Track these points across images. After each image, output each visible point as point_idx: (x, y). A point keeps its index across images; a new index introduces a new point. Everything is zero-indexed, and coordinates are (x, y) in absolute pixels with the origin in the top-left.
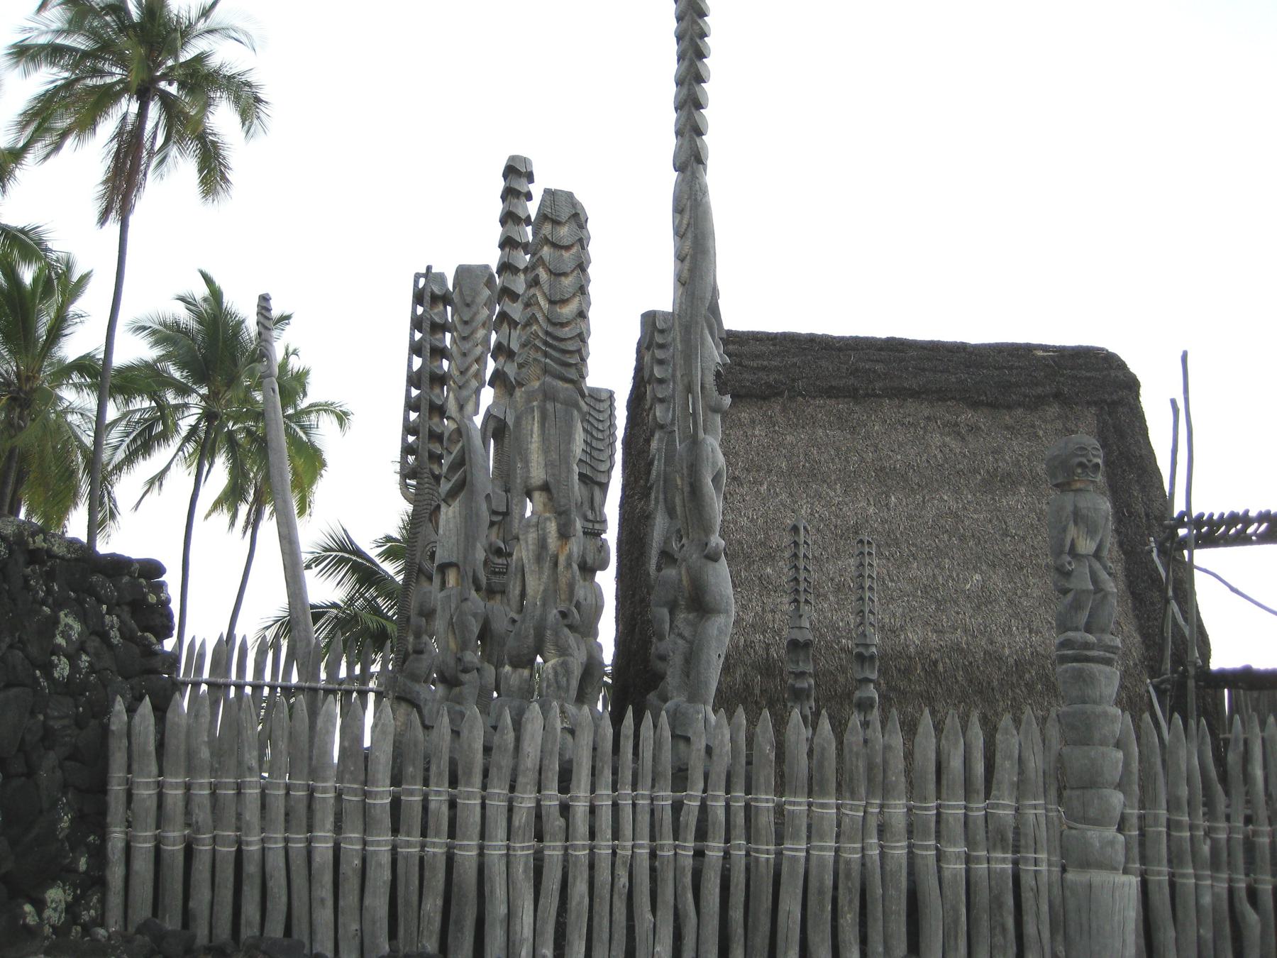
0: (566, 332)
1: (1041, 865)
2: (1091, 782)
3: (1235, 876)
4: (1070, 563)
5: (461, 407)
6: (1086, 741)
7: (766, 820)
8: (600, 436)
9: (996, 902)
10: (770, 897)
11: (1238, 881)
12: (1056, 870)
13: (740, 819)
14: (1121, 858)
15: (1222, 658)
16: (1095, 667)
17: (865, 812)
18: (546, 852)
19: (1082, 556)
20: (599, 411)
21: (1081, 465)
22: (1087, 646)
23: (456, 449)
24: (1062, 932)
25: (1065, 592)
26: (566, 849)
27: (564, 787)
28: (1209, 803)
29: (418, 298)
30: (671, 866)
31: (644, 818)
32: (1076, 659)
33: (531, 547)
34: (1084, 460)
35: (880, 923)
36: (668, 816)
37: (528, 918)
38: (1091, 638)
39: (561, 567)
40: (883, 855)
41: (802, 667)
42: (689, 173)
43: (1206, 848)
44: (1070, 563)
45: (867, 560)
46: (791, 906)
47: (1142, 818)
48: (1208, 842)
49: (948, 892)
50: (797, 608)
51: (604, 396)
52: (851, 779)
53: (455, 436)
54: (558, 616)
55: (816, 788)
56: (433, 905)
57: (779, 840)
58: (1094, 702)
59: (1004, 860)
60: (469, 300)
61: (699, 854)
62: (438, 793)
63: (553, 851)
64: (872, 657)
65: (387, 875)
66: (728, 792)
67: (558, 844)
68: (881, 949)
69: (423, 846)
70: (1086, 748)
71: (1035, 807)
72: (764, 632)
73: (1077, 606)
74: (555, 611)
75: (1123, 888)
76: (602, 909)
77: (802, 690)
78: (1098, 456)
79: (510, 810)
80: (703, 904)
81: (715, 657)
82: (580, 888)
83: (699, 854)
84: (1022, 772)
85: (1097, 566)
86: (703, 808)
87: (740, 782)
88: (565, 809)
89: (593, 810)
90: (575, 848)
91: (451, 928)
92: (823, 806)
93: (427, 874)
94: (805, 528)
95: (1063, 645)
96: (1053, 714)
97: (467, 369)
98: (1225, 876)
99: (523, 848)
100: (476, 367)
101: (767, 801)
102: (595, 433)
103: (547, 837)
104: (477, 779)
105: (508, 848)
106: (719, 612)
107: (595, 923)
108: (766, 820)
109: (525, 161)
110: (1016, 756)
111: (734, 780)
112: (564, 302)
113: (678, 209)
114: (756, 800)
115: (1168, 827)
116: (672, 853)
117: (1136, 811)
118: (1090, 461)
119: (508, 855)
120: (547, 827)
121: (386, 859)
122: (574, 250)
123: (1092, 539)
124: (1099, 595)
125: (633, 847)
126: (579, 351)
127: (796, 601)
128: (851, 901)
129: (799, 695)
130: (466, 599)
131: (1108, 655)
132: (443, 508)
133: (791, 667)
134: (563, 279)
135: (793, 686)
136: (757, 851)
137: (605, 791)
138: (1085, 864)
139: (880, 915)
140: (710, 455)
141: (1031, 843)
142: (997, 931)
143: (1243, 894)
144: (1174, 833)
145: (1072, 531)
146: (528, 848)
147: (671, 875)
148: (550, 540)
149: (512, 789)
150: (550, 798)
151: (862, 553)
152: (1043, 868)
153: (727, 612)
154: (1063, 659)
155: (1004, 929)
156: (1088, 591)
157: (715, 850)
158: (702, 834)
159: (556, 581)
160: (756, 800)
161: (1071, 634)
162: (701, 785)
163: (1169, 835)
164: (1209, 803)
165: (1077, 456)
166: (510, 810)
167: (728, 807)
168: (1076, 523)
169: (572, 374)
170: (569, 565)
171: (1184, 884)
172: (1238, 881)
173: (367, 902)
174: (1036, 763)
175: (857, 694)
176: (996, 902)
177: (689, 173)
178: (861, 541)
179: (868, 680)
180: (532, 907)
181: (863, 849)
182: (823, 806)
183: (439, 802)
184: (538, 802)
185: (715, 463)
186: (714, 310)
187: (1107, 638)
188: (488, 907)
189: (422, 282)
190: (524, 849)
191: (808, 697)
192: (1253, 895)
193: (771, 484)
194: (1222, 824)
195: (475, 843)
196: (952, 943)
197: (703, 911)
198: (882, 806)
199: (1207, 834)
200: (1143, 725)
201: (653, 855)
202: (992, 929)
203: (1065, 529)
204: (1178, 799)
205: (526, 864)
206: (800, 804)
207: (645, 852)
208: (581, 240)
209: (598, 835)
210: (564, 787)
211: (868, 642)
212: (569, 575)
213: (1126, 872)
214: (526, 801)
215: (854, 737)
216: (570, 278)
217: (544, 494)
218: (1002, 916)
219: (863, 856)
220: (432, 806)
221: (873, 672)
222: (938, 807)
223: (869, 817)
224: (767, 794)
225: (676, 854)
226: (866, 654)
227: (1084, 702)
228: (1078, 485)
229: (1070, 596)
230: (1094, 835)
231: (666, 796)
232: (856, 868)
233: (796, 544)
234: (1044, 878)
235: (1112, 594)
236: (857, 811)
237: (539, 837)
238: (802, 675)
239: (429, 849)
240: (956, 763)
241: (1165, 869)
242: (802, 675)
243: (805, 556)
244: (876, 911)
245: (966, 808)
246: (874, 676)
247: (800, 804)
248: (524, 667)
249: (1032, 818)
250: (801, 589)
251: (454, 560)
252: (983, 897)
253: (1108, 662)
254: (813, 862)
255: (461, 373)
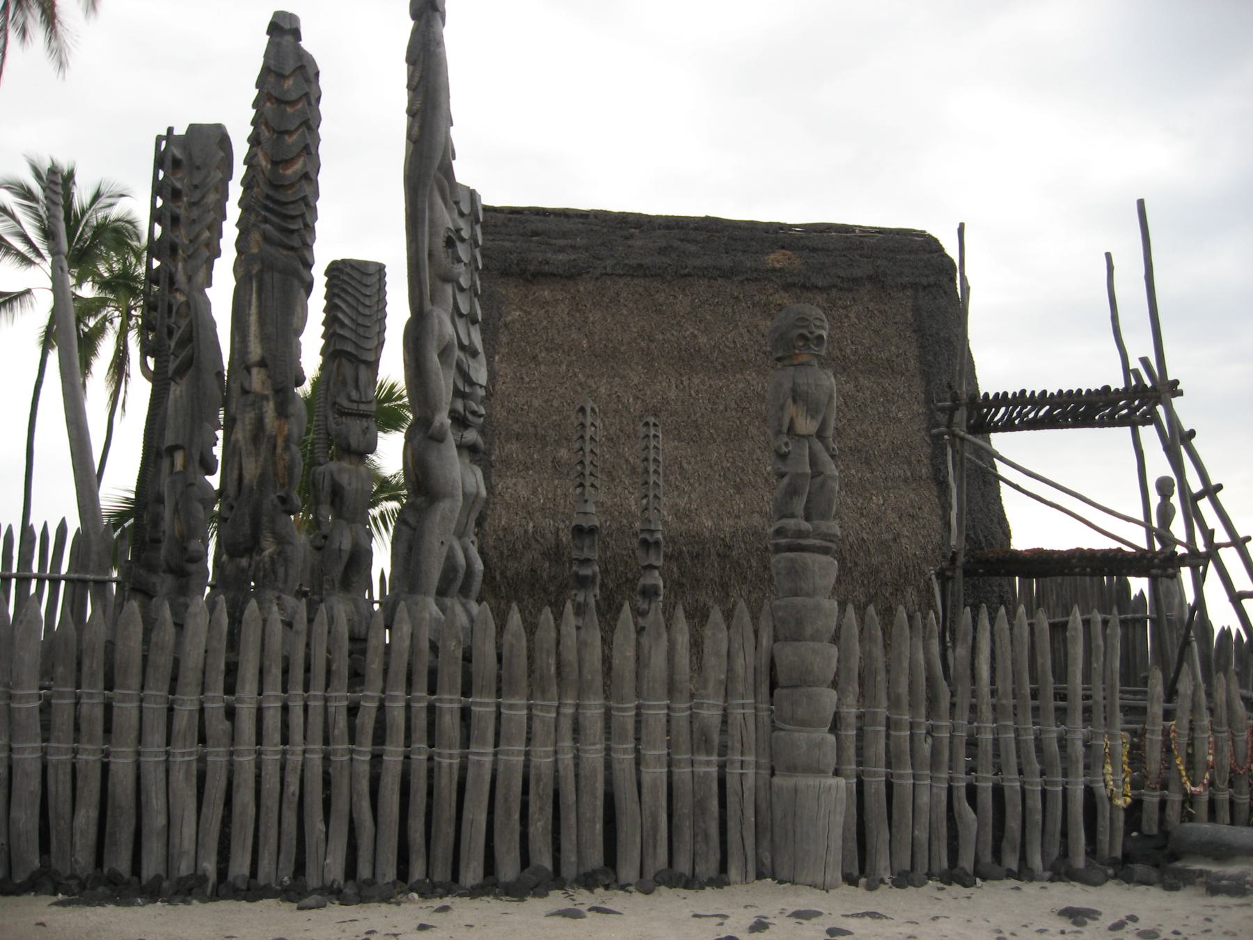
0: (289, 195)
1: (746, 771)
2: (804, 680)
3: (955, 775)
4: (786, 444)
5: (190, 279)
6: (797, 637)
7: (450, 723)
8: (367, 312)
9: (699, 806)
10: (454, 804)
11: (958, 780)
12: (765, 773)
13: (421, 721)
14: (831, 759)
15: (1021, 541)
16: (808, 556)
17: (558, 713)
18: (209, 759)
19: (803, 436)
20: (367, 286)
21: (802, 337)
22: (800, 534)
23: (184, 323)
24: (769, 835)
25: (782, 476)
26: (231, 754)
27: (230, 689)
28: (933, 701)
29: (159, 162)
30: (346, 773)
31: (316, 720)
32: (790, 549)
33: (248, 428)
34: (805, 332)
35: (574, 831)
36: (342, 722)
37: (189, 830)
38: (806, 526)
39: (279, 450)
40: (577, 758)
41: (586, 553)
42: (423, 22)
43: (926, 747)
44: (786, 444)
45: (653, 443)
46: (476, 814)
47: (860, 717)
48: (930, 740)
49: (646, 797)
50: (582, 494)
51: (371, 270)
52: (542, 678)
53: (183, 310)
54: (276, 501)
55: (504, 688)
56: (87, 816)
57: (466, 742)
58: (808, 595)
59: (708, 763)
60: (198, 162)
61: (377, 758)
62: (91, 696)
63: (217, 757)
64: (657, 543)
65: (35, 784)
66: (408, 692)
67: (222, 749)
68: (573, 859)
69: (75, 752)
70: (796, 644)
71: (743, 706)
72: (553, 516)
73: (793, 491)
74: (273, 496)
75: (835, 792)
76: (270, 818)
77: (585, 578)
78: (823, 328)
79: (171, 710)
80: (380, 812)
81: (437, 544)
82: (244, 797)
83: (377, 758)
84: (730, 670)
85: (818, 446)
86: (381, 708)
87: (422, 681)
88: (231, 713)
89: (285, 709)
90: (240, 754)
91: (107, 841)
92: (511, 707)
93: (80, 784)
94: (593, 410)
95: (779, 532)
96: (766, 608)
97: (197, 236)
98: (945, 775)
99: (183, 754)
100: (207, 234)
101: (451, 701)
102: (360, 309)
103: (210, 742)
104: (135, 681)
105: (168, 753)
106: (444, 496)
107: (261, 834)
108: (450, 723)
109: (293, 18)
110: (724, 651)
111: (415, 678)
112: (288, 162)
113: (412, 59)
114: (440, 700)
115: (888, 727)
116: (346, 758)
117: (854, 710)
118: (811, 333)
119: (167, 761)
120: (210, 731)
121: (36, 768)
122: (300, 106)
123: (813, 417)
124: (819, 480)
125: (305, 752)
126: (302, 216)
127: (581, 485)
128: (541, 809)
129: (583, 582)
130: (192, 484)
131: (824, 543)
132: (173, 387)
133: (576, 554)
134: (287, 137)
135: (576, 574)
136: (440, 755)
137: (273, 690)
138: (792, 769)
139: (573, 820)
140: (436, 327)
141: (738, 745)
142: (699, 838)
143: (963, 793)
144: (892, 733)
145: (791, 409)
146: (191, 754)
147: (346, 781)
148: (267, 420)
149: (172, 691)
150: (213, 699)
151: (647, 436)
152: (750, 772)
153: (452, 496)
154: (778, 549)
155: (706, 836)
156: (804, 475)
157: (393, 755)
158: (380, 736)
159: (275, 464)
160: (440, 700)
161: (785, 521)
162: (380, 684)
163: (888, 736)
164: (933, 701)
165: (799, 327)
166: (171, 710)
167: (408, 707)
168: (795, 401)
169: (296, 242)
170: (287, 447)
171: (900, 785)
172: (958, 780)
173: (13, 814)
174: (744, 662)
175: (642, 581)
176: (699, 806)
177: (423, 22)
178: (647, 424)
179: (651, 567)
180: (194, 818)
181: (556, 752)
182: (511, 707)
183: (92, 709)
184: (202, 703)
185: (441, 336)
186: (448, 172)
187: (824, 526)
188: (145, 820)
189: (164, 143)
190: (185, 754)
191: (593, 582)
192: (972, 794)
193: (570, 364)
194: (946, 723)
195: (130, 749)
196: (651, 851)
197: (380, 820)
198: (577, 706)
199: (928, 733)
200: (867, 619)
201: (326, 758)
202: (695, 836)
203: (782, 408)
204: (898, 697)
205: (188, 771)
206: (486, 705)
207: (316, 758)
208: (307, 95)
209: (265, 741)
210: (230, 689)
211: (653, 527)
212: (287, 457)
213: (837, 773)
214: (187, 705)
215: (546, 632)
216: (295, 137)
217: (263, 371)
218: (705, 822)
219: (556, 761)
220: (84, 709)
221: (658, 558)
222: (638, 707)
223: (562, 718)
224: (450, 693)
225: (351, 759)
226: (651, 540)
227: (796, 595)
228: (804, 358)
229: (786, 480)
230: (801, 737)
231: (341, 697)
232: (547, 773)
233: (583, 425)
234: (750, 782)
235: (832, 477)
236: (548, 712)
237: (202, 740)
238: (586, 562)
239: (82, 757)
240: (658, 660)
241: (883, 770)
242: (586, 562)
243: (592, 438)
244: (569, 819)
245: (669, 708)
246: (660, 563)
247: (486, 705)
248: (242, 557)
249: (740, 718)
250: (587, 473)
251: (180, 442)
252: (684, 806)
253: (825, 551)
254: (501, 768)
255: (191, 241)
